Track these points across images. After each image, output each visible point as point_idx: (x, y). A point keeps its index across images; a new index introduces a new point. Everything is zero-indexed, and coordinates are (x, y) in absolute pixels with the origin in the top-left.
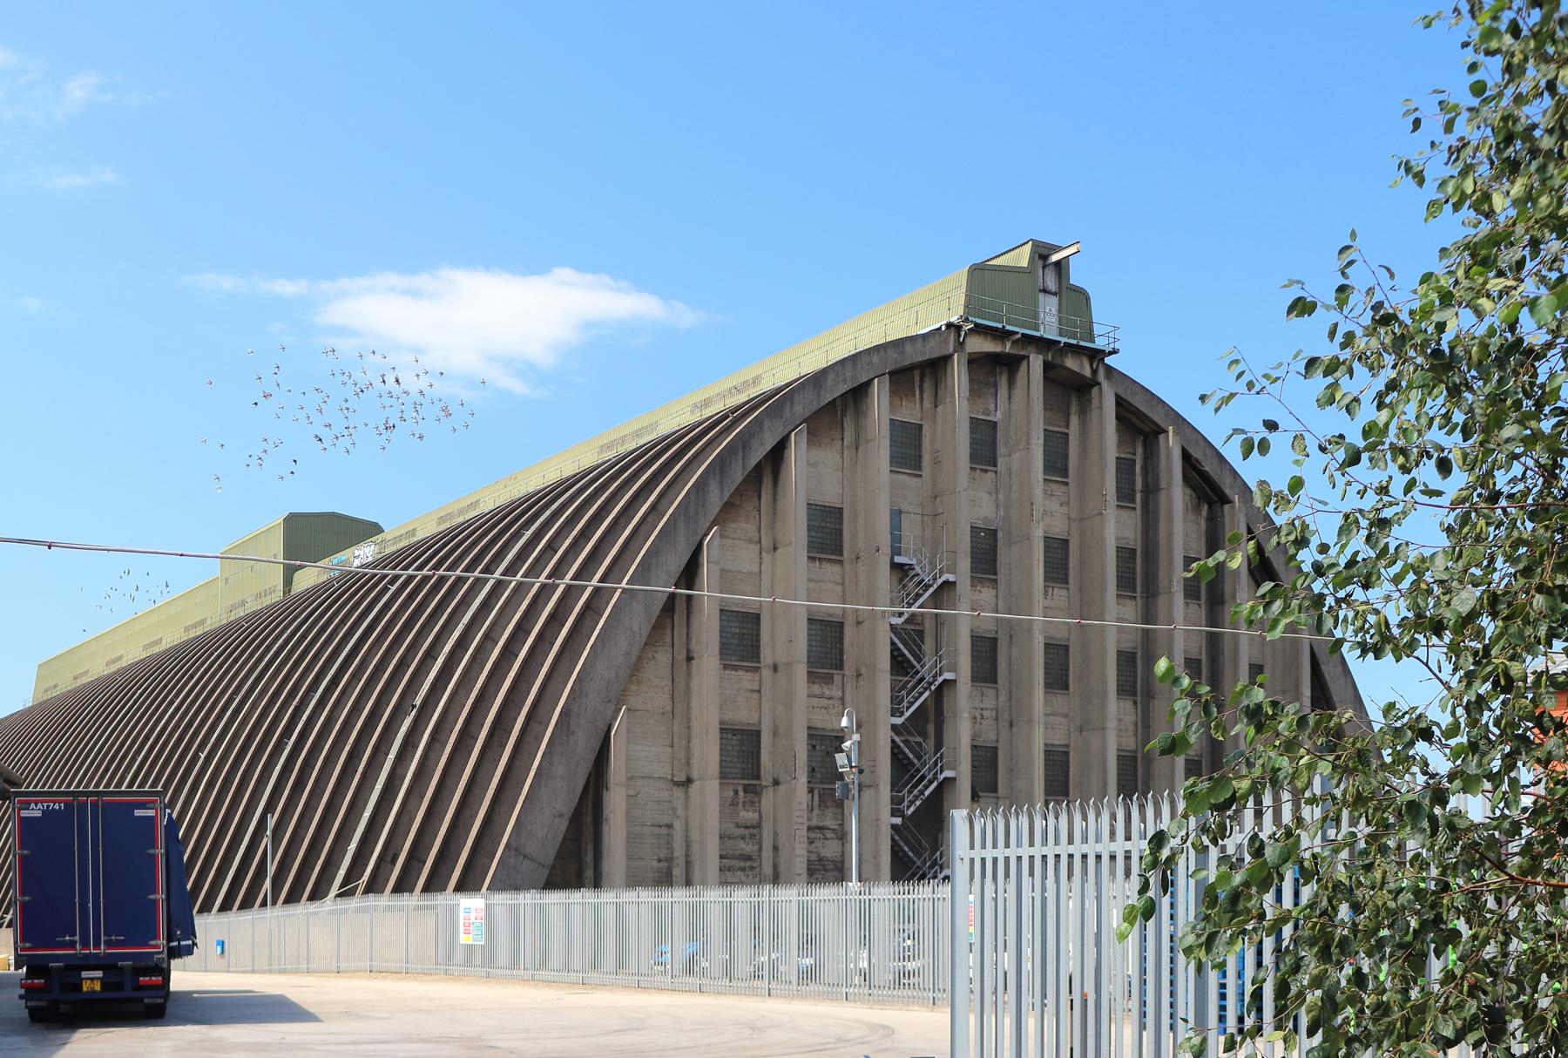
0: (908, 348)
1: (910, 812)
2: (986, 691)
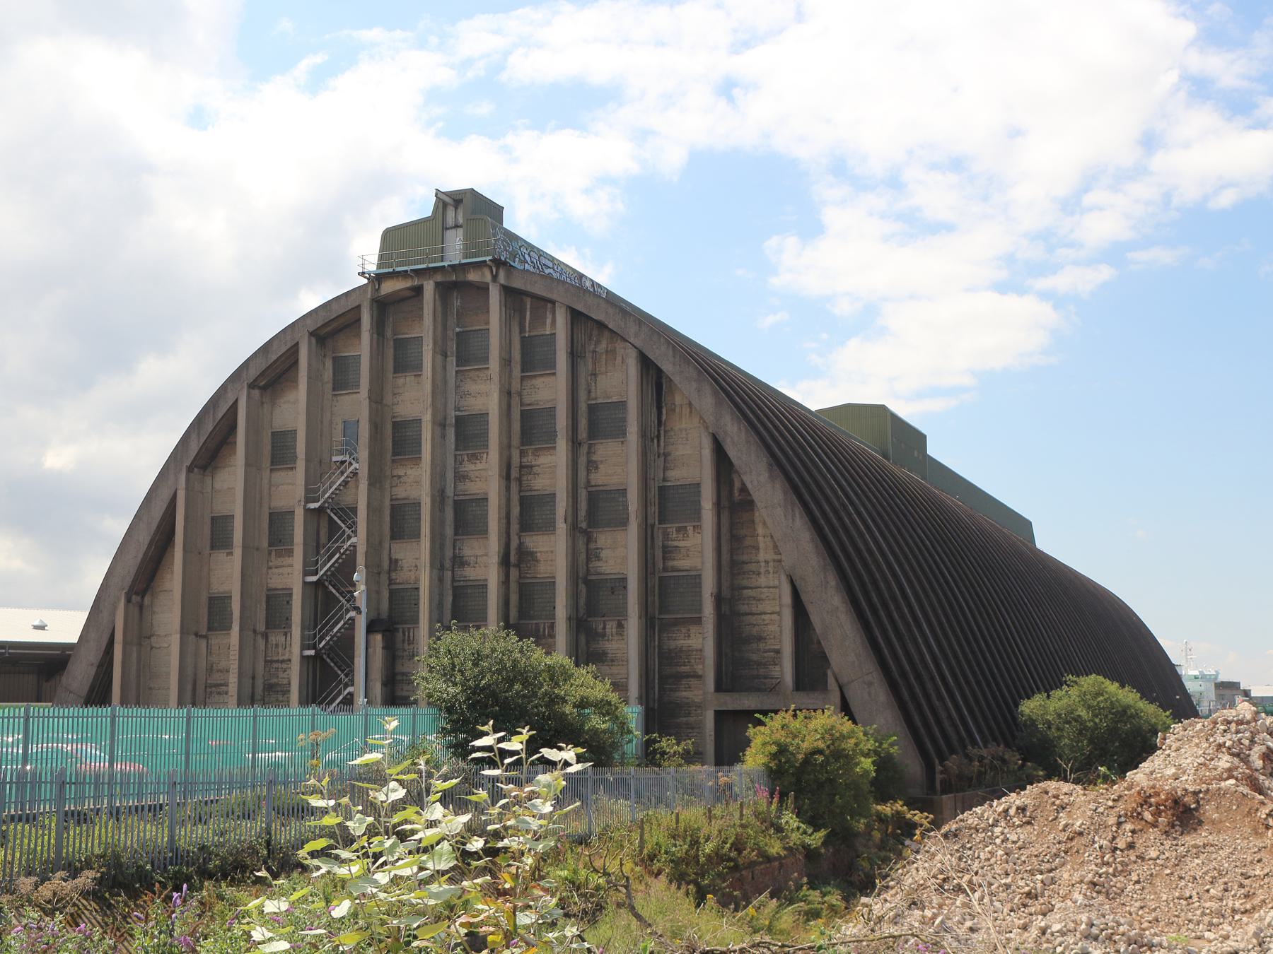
0: (334, 306)
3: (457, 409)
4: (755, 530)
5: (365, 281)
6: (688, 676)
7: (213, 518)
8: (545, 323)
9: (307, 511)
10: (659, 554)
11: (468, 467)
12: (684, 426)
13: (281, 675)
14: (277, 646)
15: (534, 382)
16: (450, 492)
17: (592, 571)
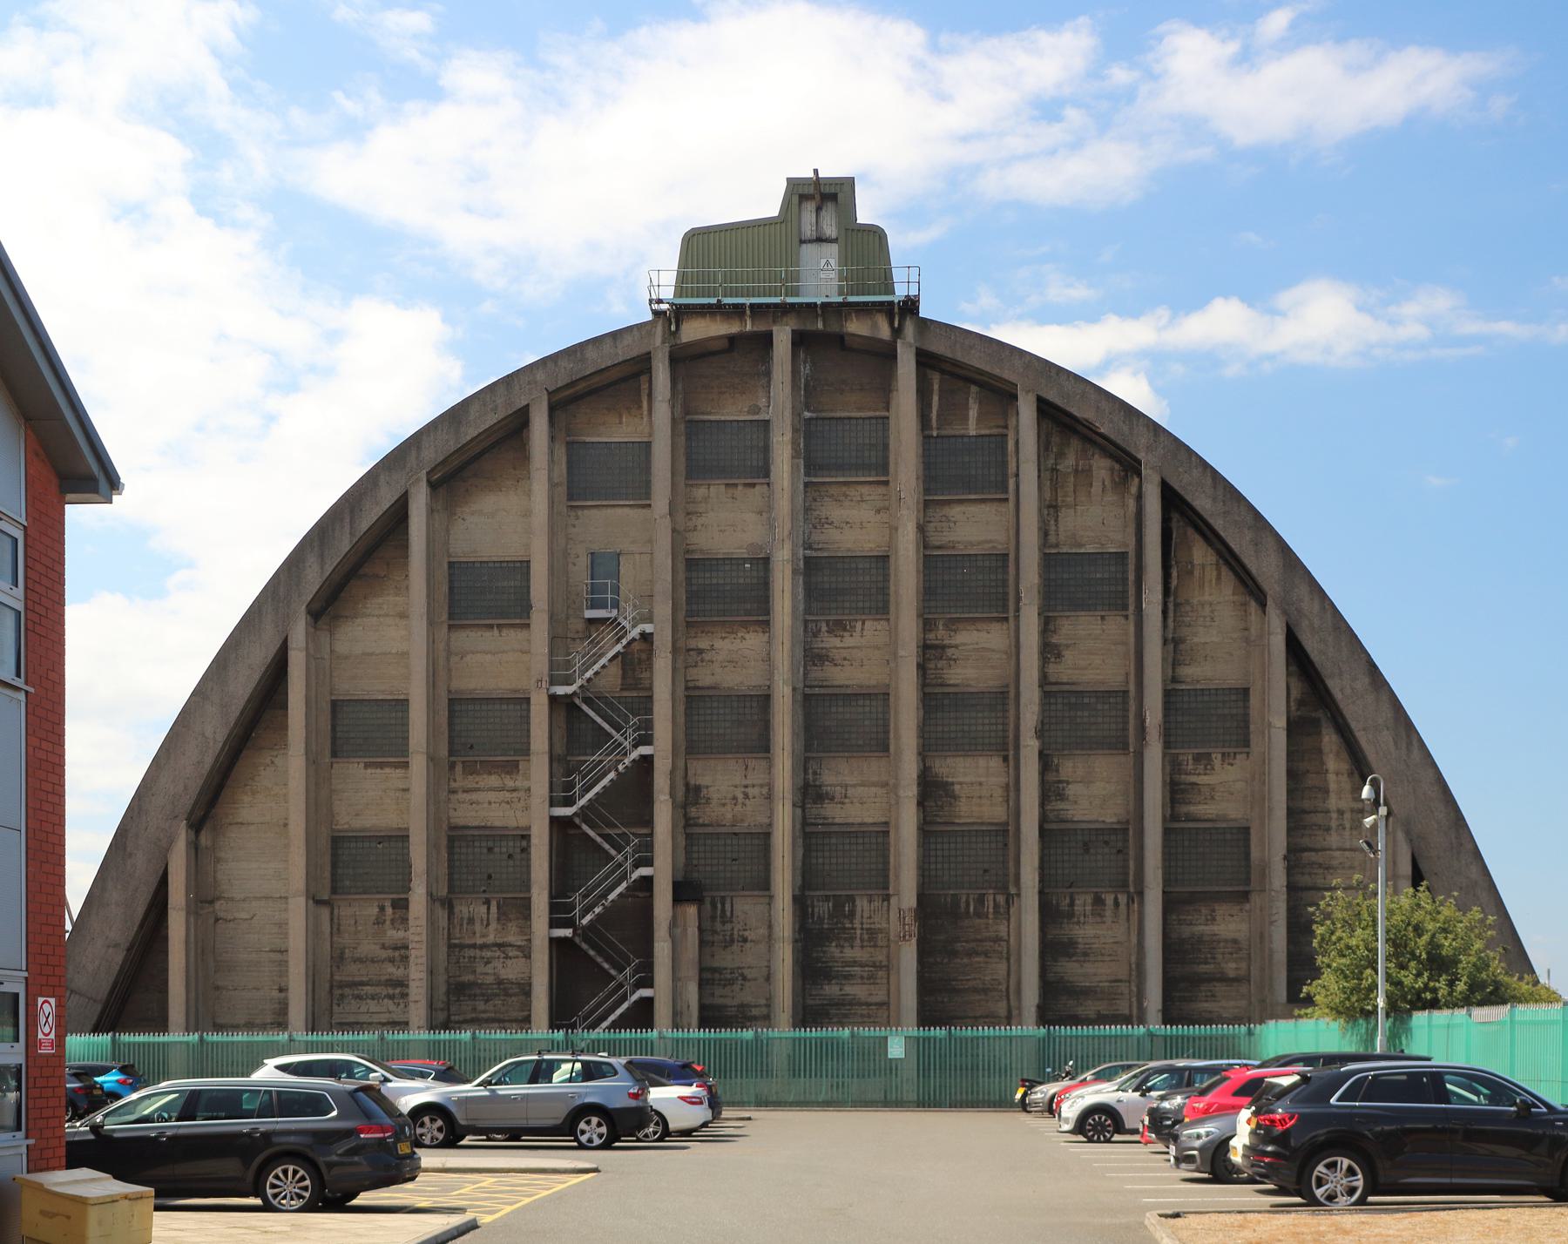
0: (591, 354)
1: (585, 921)
2: (752, 763)
4: (1323, 763)
6: (1211, 979)
7: (334, 704)
8: (966, 418)
11: (830, 642)
12: (1207, 598)
13: (480, 968)
14: (471, 921)
15: (947, 511)
17: (1051, 816)
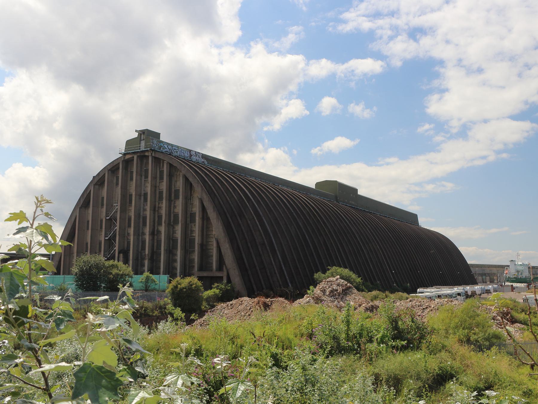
3: (144, 191)
5: (121, 155)
9: (106, 219)
10: (189, 232)
16: (142, 214)
